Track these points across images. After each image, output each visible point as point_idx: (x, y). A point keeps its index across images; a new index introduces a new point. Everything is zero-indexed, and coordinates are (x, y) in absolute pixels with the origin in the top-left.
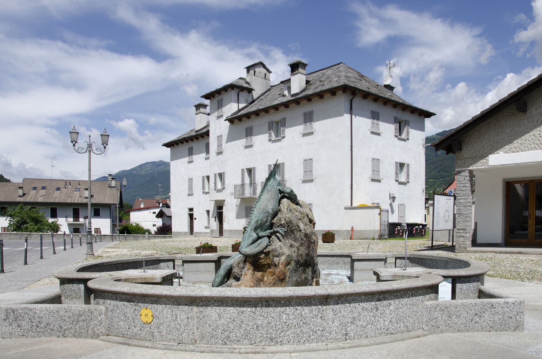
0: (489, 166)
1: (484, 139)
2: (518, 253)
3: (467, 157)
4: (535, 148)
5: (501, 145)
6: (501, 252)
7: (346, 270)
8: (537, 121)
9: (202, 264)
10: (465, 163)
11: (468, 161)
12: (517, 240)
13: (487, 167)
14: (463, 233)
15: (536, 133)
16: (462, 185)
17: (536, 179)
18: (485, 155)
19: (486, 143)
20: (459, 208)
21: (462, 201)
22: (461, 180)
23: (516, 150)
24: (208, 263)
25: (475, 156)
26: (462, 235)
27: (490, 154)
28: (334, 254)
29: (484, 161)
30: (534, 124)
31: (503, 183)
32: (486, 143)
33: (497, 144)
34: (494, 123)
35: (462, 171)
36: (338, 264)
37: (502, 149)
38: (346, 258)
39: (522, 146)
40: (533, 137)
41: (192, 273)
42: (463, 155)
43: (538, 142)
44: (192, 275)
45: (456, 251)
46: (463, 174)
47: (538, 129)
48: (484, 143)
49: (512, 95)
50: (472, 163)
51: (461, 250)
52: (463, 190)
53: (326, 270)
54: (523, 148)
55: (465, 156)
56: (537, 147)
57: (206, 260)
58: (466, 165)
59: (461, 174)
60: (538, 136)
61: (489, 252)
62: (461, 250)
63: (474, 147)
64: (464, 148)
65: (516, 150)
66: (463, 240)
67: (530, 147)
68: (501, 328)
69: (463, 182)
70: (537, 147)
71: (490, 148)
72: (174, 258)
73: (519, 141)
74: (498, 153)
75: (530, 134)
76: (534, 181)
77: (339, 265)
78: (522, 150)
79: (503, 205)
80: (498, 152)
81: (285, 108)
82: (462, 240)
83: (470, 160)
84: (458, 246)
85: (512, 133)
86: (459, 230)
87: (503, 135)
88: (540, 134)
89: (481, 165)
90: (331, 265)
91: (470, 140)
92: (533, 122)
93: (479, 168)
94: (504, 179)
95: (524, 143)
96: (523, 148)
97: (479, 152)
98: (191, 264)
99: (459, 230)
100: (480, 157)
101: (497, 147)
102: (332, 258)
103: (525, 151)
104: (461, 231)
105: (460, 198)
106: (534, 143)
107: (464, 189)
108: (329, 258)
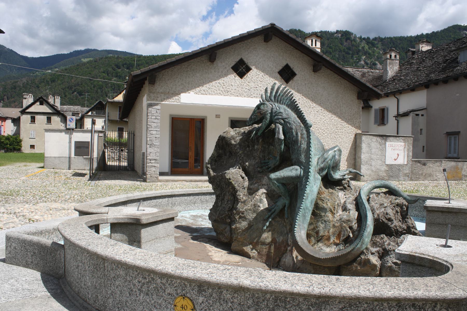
0: (181, 103)
1: (177, 78)
2: (191, 181)
3: (160, 91)
4: (220, 93)
5: (192, 86)
6: (191, 181)
7: (203, 210)
8: (222, 72)
9: (161, 226)
10: (158, 97)
11: (161, 95)
12: (180, 170)
13: (178, 103)
14: (155, 163)
15: (221, 81)
16: (154, 117)
17: (196, 118)
18: (177, 92)
19: (178, 82)
20: (151, 139)
21: (154, 132)
22: (153, 112)
23: (204, 93)
24: (167, 223)
25: (167, 92)
26: (153, 165)
27: (182, 92)
28: (193, 193)
29: (177, 98)
30: (220, 74)
31: (170, 118)
32: (178, 82)
33: (189, 84)
34: (186, 66)
35: (157, 104)
36: (194, 204)
37: (193, 90)
38: (203, 196)
39: (210, 90)
40: (219, 85)
41: (150, 242)
42: (156, 90)
43: (222, 90)
44: (150, 246)
45: (148, 181)
46: (156, 107)
47: (223, 79)
48: (177, 82)
49: (211, 47)
50: (165, 98)
51: (153, 179)
52: (154, 122)
53: (183, 212)
54: (210, 92)
55: (158, 91)
56: (222, 93)
57: (168, 217)
58: (159, 99)
59: (153, 107)
60: (222, 84)
61: (180, 181)
62: (153, 179)
63: (167, 83)
64: (157, 83)
65: (204, 93)
66: (155, 170)
67: (216, 92)
68: (113, 252)
69: (155, 114)
70: (222, 93)
71: (182, 87)
72: (97, 223)
73: (207, 85)
74: (190, 93)
75: (216, 81)
76: (194, 119)
77: (196, 205)
78: (210, 94)
79: (170, 137)
80: (189, 92)
81: (428, 34)
82: (154, 170)
83: (162, 95)
84: (150, 175)
85: (202, 78)
86: (150, 160)
87: (194, 77)
88: (224, 83)
89: (173, 101)
90: (188, 206)
91: (164, 76)
92: (218, 72)
93: (171, 103)
94: (206, 117)
95: (212, 88)
96: (210, 92)
97: (172, 89)
98: (149, 228)
99: (150, 160)
100: (173, 94)
101: (188, 87)
102: (188, 197)
103: (212, 95)
104: (152, 161)
105: (152, 129)
106: (219, 90)
107: (156, 121)
108: (186, 198)
